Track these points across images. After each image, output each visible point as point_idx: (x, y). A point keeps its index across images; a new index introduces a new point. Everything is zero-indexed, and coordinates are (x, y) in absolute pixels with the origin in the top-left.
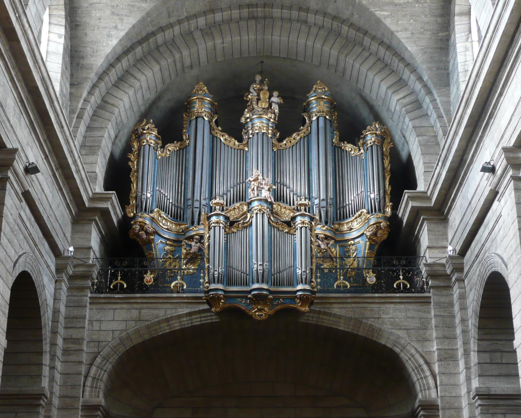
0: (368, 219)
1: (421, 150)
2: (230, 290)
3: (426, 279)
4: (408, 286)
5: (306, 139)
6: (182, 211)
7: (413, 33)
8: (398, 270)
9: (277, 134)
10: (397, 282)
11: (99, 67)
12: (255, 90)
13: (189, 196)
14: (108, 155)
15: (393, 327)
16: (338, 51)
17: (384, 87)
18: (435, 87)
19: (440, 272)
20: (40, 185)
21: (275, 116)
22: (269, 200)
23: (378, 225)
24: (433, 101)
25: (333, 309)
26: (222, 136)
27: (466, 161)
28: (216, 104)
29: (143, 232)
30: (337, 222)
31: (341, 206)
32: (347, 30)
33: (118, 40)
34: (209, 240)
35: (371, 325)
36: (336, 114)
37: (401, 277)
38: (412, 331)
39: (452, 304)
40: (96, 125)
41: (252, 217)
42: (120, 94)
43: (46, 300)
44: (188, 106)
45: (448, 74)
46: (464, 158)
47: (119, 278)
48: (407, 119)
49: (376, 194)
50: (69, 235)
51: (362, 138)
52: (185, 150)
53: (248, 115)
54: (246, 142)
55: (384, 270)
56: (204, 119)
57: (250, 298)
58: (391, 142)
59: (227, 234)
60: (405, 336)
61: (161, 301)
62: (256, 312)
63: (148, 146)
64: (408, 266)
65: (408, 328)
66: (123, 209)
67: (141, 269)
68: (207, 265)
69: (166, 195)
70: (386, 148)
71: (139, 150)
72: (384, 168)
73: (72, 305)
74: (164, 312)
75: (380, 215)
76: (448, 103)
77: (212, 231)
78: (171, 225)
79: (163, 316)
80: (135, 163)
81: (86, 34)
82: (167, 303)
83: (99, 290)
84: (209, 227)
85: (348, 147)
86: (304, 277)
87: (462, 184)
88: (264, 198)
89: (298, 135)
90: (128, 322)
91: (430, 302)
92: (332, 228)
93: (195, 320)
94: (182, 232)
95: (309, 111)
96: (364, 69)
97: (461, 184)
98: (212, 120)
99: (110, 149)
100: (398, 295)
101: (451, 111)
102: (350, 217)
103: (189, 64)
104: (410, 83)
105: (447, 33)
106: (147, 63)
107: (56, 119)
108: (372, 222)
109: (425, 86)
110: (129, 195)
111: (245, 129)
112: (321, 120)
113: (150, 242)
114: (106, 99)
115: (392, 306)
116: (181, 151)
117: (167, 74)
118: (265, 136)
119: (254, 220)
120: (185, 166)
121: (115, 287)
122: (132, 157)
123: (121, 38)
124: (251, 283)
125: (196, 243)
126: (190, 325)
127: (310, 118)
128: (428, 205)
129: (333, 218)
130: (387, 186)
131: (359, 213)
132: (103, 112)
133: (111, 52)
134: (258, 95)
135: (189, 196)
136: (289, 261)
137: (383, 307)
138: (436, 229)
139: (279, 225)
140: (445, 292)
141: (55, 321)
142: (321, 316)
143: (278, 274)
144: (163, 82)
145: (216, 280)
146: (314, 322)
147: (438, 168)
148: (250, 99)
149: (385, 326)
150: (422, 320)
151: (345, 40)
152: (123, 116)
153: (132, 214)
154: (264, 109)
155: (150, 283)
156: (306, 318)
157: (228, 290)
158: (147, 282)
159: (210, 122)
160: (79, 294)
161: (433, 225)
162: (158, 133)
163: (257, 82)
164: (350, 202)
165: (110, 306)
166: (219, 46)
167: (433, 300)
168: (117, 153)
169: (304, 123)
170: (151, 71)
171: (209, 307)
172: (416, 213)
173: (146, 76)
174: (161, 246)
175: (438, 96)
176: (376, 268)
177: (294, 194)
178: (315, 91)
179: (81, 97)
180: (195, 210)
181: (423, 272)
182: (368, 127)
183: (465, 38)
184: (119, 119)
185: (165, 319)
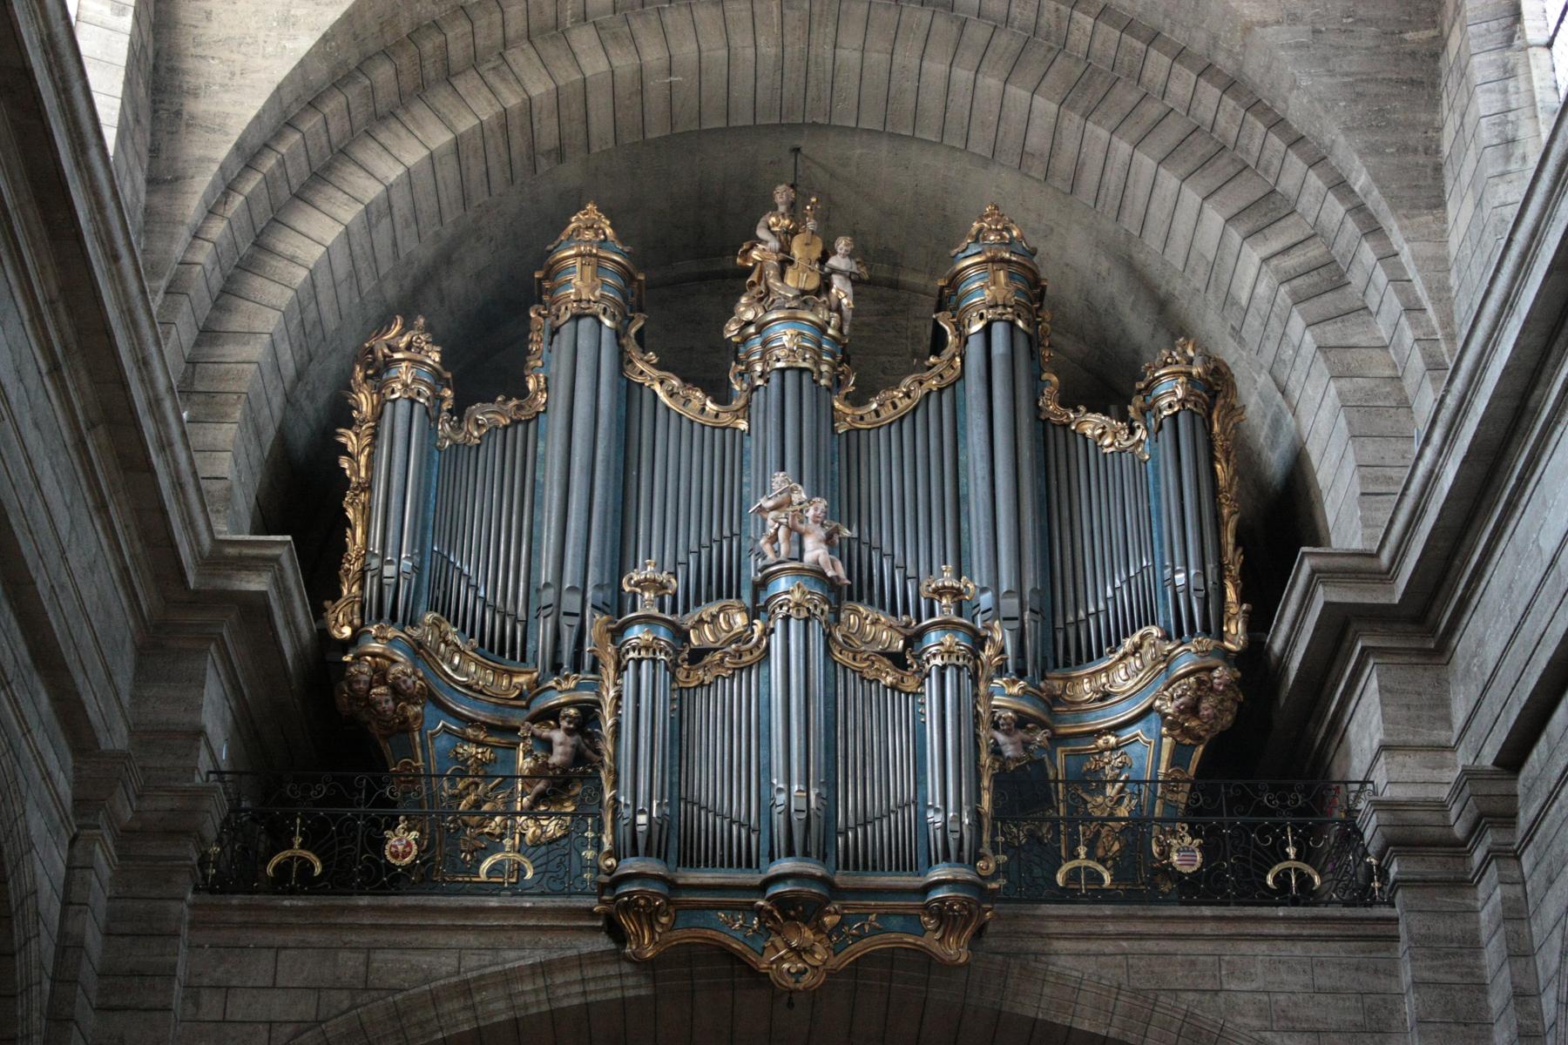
0: (1168, 659)
1: (1349, 423)
2: (692, 881)
3: (1380, 856)
7: (1316, 32)
8: (1278, 825)
9: (848, 378)
10: (1277, 868)
12: (773, 233)
13: (546, 574)
14: (270, 433)
15: (1267, 1024)
16: (1058, 98)
18: (1393, 208)
20: (29, 461)
21: (842, 319)
24: (1388, 257)
26: (662, 383)
27: (1536, 413)
29: (382, 690)
30: (1056, 674)
31: (1071, 618)
32: (1089, 28)
33: (318, 35)
34: (618, 707)
37: (1291, 851)
39: (1473, 945)
41: (768, 632)
43: (36, 892)
44: (547, 285)
45: (1438, 169)
47: (298, 840)
48: (1297, 323)
49: (1192, 572)
50: (124, 681)
51: (1140, 392)
52: (532, 425)
53: (749, 316)
54: (742, 402)
55: (1232, 825)
56: (600, 323)
61: (442, 922)
63: (407, 404)
64: (1313, 814)
65: (1320, 1026)
66: (318, 612)
68: (608, 795)
69: (466, 570)
71: (378, 416)
75: (1208, 643)
76: (1439, 265)
77: (629, 675)
78: (481, 673)
79: (449, 975)
80: (363, 460)
81: (208, 15)
82: (464, 927)
83: (220, 886)
84: (618, 663)
85: (1091, 424)
86: (952, 838)
87: (1516, 507)
88: (814, 567)
91: (1396, 938)
93: (561, 992)
95: (957, 308)
97: (1511, 506)
98: (626, 328)
99: (278, 414)
100: (1281, 912)
101: (1449, 289)
102: (1100, 655)
103: (554, 142)
104: (1307, 202)
105: (1433, 33)
106: (412, 127)
107: (92, 219)
109: (1358, 209)
111: (738, 362)
112: (999, 331)
115: (1262, 947)
116: (520, 428)
117: (476, 170)
118: (806, 377)
119: (776, 641)
120: (534, 480)
121: (282, 869)
122: (349, 439)
123: (325, 28)
124: (764, 860)
125: (569, 732)
126: (545, 1008)
127: (960, 327)
128: (1382, 600)
129: (1044, 658)
131: (1136, 638)
133: (290, 78)
134: (785, 248)
135: (546, 574)
136: (901, 785)
140: (1446, 901)
141: (64, 978)
144: (465, 199)
147: (1429, 454)
148: (756, 263)
149: (1239, 1020)
150: (1368, 1000)
151: (1083, 67)
152: (325, 307)
153: (347, 631)
154: (804, 292)
157: (681, 881)
158: (395, 855)
159: (618, 334)
162: (442, 362)
163: (782, 209)
164: (1101, 606)
165: (260, 937)
167: (1409, 932)
168: (301, 436)
169: (938, 342)
171: (613, 946)
172: (1339, 627)
174: (443, 742)
175: (1407, 240)
176: (1196, 817)
177: (906, 578)
178: (976, 241)
180: (565, 621)
181: (1367, 835)
183: (1500, 36)
184: (311, 315)
185: (456, 985)
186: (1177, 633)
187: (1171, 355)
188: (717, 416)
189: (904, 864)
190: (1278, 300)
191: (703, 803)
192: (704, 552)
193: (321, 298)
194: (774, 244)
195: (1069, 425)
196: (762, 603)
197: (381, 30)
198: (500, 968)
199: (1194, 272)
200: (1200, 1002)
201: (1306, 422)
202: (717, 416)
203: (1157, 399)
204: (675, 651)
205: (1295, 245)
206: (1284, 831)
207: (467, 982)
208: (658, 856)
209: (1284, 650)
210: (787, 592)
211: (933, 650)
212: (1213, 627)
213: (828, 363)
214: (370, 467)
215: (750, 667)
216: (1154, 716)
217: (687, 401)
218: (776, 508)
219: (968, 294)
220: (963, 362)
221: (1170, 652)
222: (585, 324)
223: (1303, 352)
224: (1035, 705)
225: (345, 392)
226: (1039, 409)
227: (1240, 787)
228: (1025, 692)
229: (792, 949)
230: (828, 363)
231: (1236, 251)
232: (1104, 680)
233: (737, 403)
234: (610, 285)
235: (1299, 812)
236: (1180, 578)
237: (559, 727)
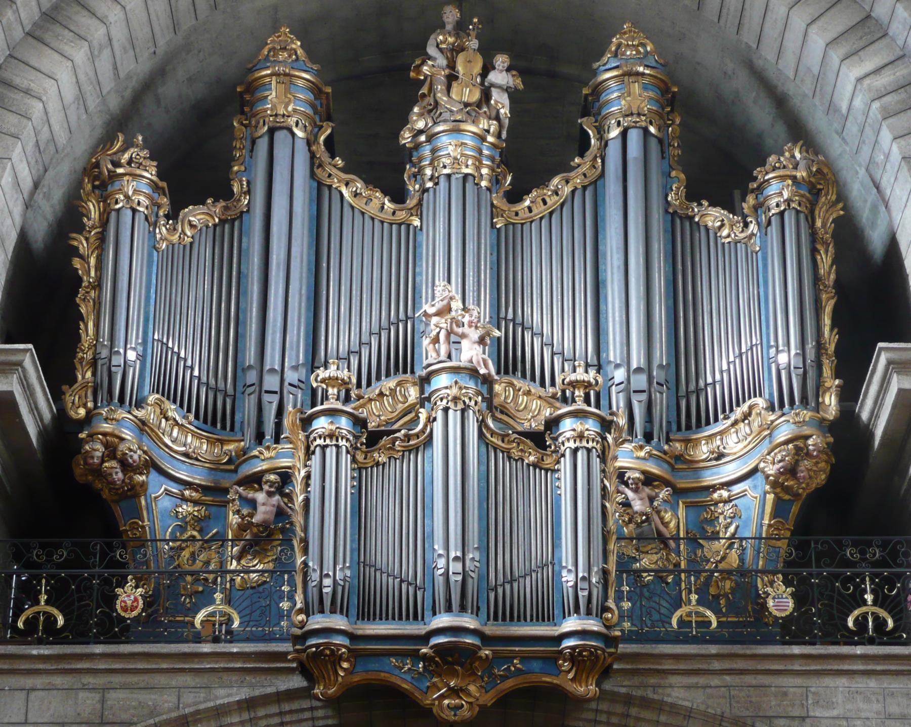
0: (771, 427)
4: (891, 623)
6: (229, 401)
8: (858, 575)
9: (505, 178)
10: (856, 612)
12: (441, 50)
13: (250, 357)
17: (817, 41)
21: (501, 126)
22: (482, 371)
23: (800, 443)
25: (669, 690)
26: (347, 185)
29: (114, 464)
30: (679, 436)
31: (692, 387)
34: (307, 485)
36: (678, 121)
37: (869, 597)
41: (431, 420)
42: (47, 60)
44: (247, 97)
47: (43, 598)
48: (886, 136)
49: (793, 352)
51: (753, 191)
52: (237, 223)
53: (421, 125)
55: (819, 575)
56: (293, 134)
57: (424, 658)
59: (360, 469)
61: (165, 666)
62: (443, 697)
64: (888, 566)
66: (57, 395)
68: (300, 560)
70: (824, 221)
71: (104, 223)
72: (816, 279)
74: (174, 699)
75: (806, 414)
77: (316, 459)
78: (196, 443)
79: (170, 710)
80: (93, 261)
84: (308, 448)
88: (468, 365)
89: (567, 182)
94: (230, 462)
95: (599, 114)
98: (316, 137)
99: (18, 220)
100: (859, 650)
102: (716, 420)
111: (414, 165)
112: (634, 137)
113: (134, 492)
115: (843, 681)
116: (227, 226)
119: (438, 427)
121: (31, 623)
122: (83, 245)
124: (428, 613)
125: (270, 494)
127: (601, 131)
129: (669, 423)
130: (827, 331)
131: (745, 408)
134: (452, 65)
135: (250, 357)
136: (539, 549)
139: (509, 442)
142: (634, 711)
143: (508, 587)
144: (175, 27)
148: (426, 77)
152: (56, 127)
153: (82, 412)
154: (466, 105)
155: (135, 613)
156: (591, 716)
157: (360, 632)
158: (125, 609)
159: (310, 143)
162: (159, 175)
163: (449, 27)
164: (718, 377)
168: (40, 232)
169: (583, 146)
176: (793, 570)
177: (553, 354)
178: (616, 55)
180: (266, 398)
182: (772, 159)
184: (45, 135)
186: (777, 405)
187: (779, 161)
190: (871, 113)
192: (384, 335)
195: (693, 217)
196: (426, 395)
198: (212, 704)
201: (897, 216)
202: (394, 213)
203: (767, 198)
204: (355, 436)
205: (886, 65)
206: (863, 581)
207: (185, 717)
208: (341, 612)
209: (870, 419)
210: (446, 388)
211: (568, 435)
212: (809, 397)
213: (488, 166)
214: (99, 266)
215: (417, 449)
216: (759, 474)
218: (438, 314)
219: (608, 102)
221: (772, 422)
223: (892, 158)
224: (659, 466)
225: (77, 203)
226: (668, 203)
227: (827, 542)
228: (650, 455)
229: (450, 689)
230: (488, 166)
231: (836, 71)
232: (719, 443)
233: (411, 202)
234: (300, 100)
235: (875, 564)
237: (261, 489)
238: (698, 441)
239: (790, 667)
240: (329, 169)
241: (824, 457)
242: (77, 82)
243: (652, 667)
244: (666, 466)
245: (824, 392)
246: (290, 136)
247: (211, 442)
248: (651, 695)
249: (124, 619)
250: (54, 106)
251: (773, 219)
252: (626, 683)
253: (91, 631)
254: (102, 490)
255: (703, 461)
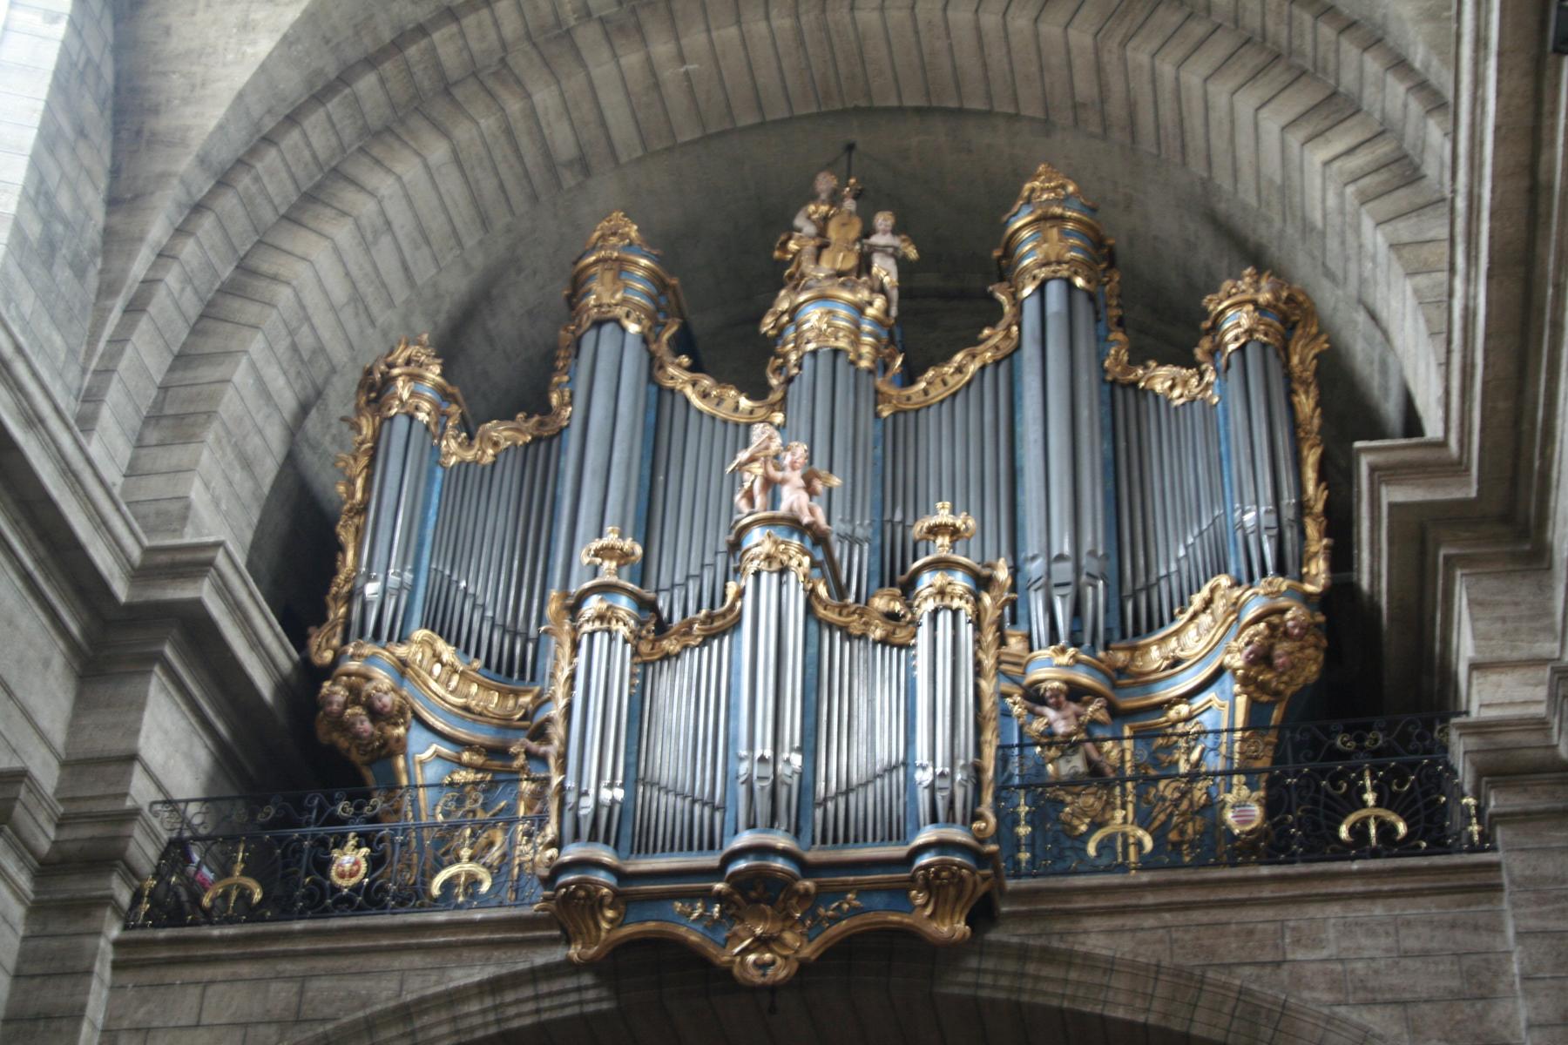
0: (1237, 607)
4: (1402, 828)
5: (1003, 370)
6: (530, 646)
9: (894, 359)
10: (1352, 818)
11: (212, 134)
14: (269, 469)
15: (1341, 997)
17: (1271, 124)
19: (1530, 753)
21: (888, 301)
22: (806, 519)
23: (1275, 619)
25: (1082, 938)
26: (694, 384)
28: (674, 281)
29: (358, 710)
30: (1123, 644)
31: (1142, 579)
33: (278, 37)
34: (572, 688)
35: (1242, 991)
36: (1117, 278)
37: (1370, 797)
38: (1426, 1008)
40: (209, 345)
41: (741, 594)
42: (303, 242)
46: (1542, 177)
48: (1367, 224)
49: (1263, 509)
52: (555, 443)
55: (1297, 773)
56: (624, 330)
57: (719, 897)
58: (1319, 333)
59: (645, 664)
60: (1396, 1030)
61: (385, 942)
62: (746, 951)
65: (1407, 996)
67: (323, 831)
70: (1302, 357)
72: (1295, 425)
73: (36, 969)
74: (394, 985)
75: (1283, 584)
79: (388, 999)
85: (1161, 378)
88: (788, 515)
89: (974, 357)
90: (251, 1031)
92: (1100, 660)
93: (512, 1011)
94: (524, 718)
96: (1193, 77)
98: (658, 336)
100: (1355, 866)
104: (1370, 96)
106: (406, 138)
108: (1250, 613)
110: (326, 590)
112: (1054, 291)
113: (386, 752)
114: (253, 262)
115: (1335, 910)
116: (543, 447)
117: (488, 186)
118: (841, 361)
123: (285, 29)
126: (492, 1030)
129: (1108, 630)
130: (1311, 488)
131: (1205, 592)
132: (236, 304)
134: (822, 233)
137: (1294, 916)
138: (1506, 598)
139: (849, 615)
142: (1031, 968)
143: (841, 801)
144: (484, 221)
145: (585, 828)
146: (1001, 995)
149: (1306, 995)
150: (1467, 962)
153: (328, 656)
155: (354, 880)
156: (969, 978)
158: (342, 875)
160: (72, 929)
161: (1489, 584)
163: (823, 196)
164: (1173, 567)
165: (187, 973)
166: (670, 74)
169: (993, 314)
170: (417, 160)
173: (399, 178)
179: (141, 239)
182: (1227, 285)
188: (751, 412)
189: (895, 833)
191: (663, 783)
193: (316, 321)
194: (810, 229)
197: (357, 33)
199: (1268, 204)
200: (1259, 977)
205: (1363, 143)
208: (607, 842)
211: (925, 593)
216: (1227, 676)
217: (720, 401)
220: (1020, 330)
221: (1238, 598)
222: (608, 329)
226: (1105, 371)
233: (775, 396)
235: (1377, 753)
236: (1249, 518)
238: (1148, 646)
239: (1256, 895)
240: (671, 370)
241: (1311, 639)
242: (347, 274)
243: (1058, 906)
244: (1101, 676)
245: (1309, 559)
246: (618, 330)
247: (504, 694)
248: (1055, 943)
249: (339, 889)
250: (312, 298)
251: (1233, 357)
252: (1022, 931)
253: (294, 904)
254: (348, 750)
255: (1156, 671)
